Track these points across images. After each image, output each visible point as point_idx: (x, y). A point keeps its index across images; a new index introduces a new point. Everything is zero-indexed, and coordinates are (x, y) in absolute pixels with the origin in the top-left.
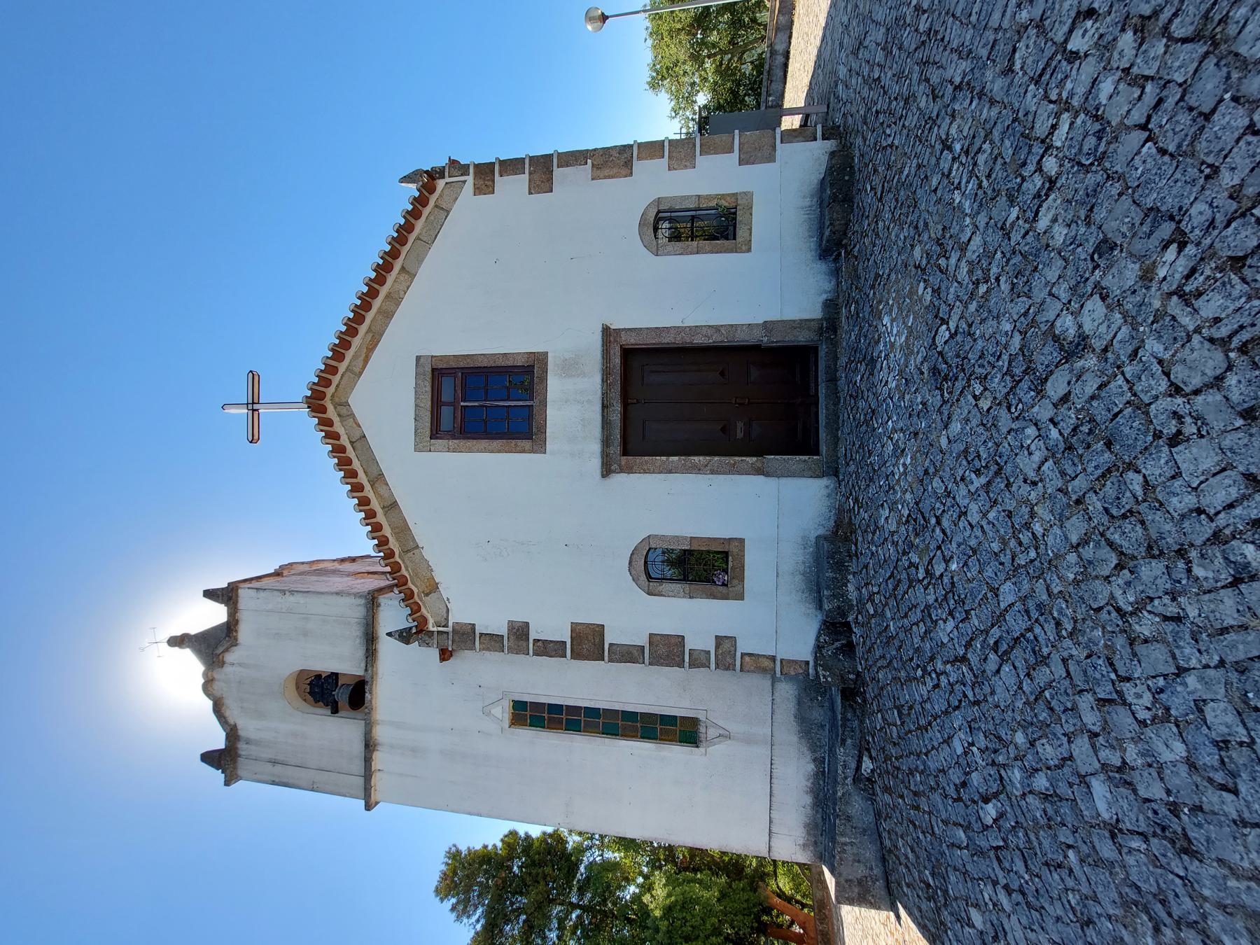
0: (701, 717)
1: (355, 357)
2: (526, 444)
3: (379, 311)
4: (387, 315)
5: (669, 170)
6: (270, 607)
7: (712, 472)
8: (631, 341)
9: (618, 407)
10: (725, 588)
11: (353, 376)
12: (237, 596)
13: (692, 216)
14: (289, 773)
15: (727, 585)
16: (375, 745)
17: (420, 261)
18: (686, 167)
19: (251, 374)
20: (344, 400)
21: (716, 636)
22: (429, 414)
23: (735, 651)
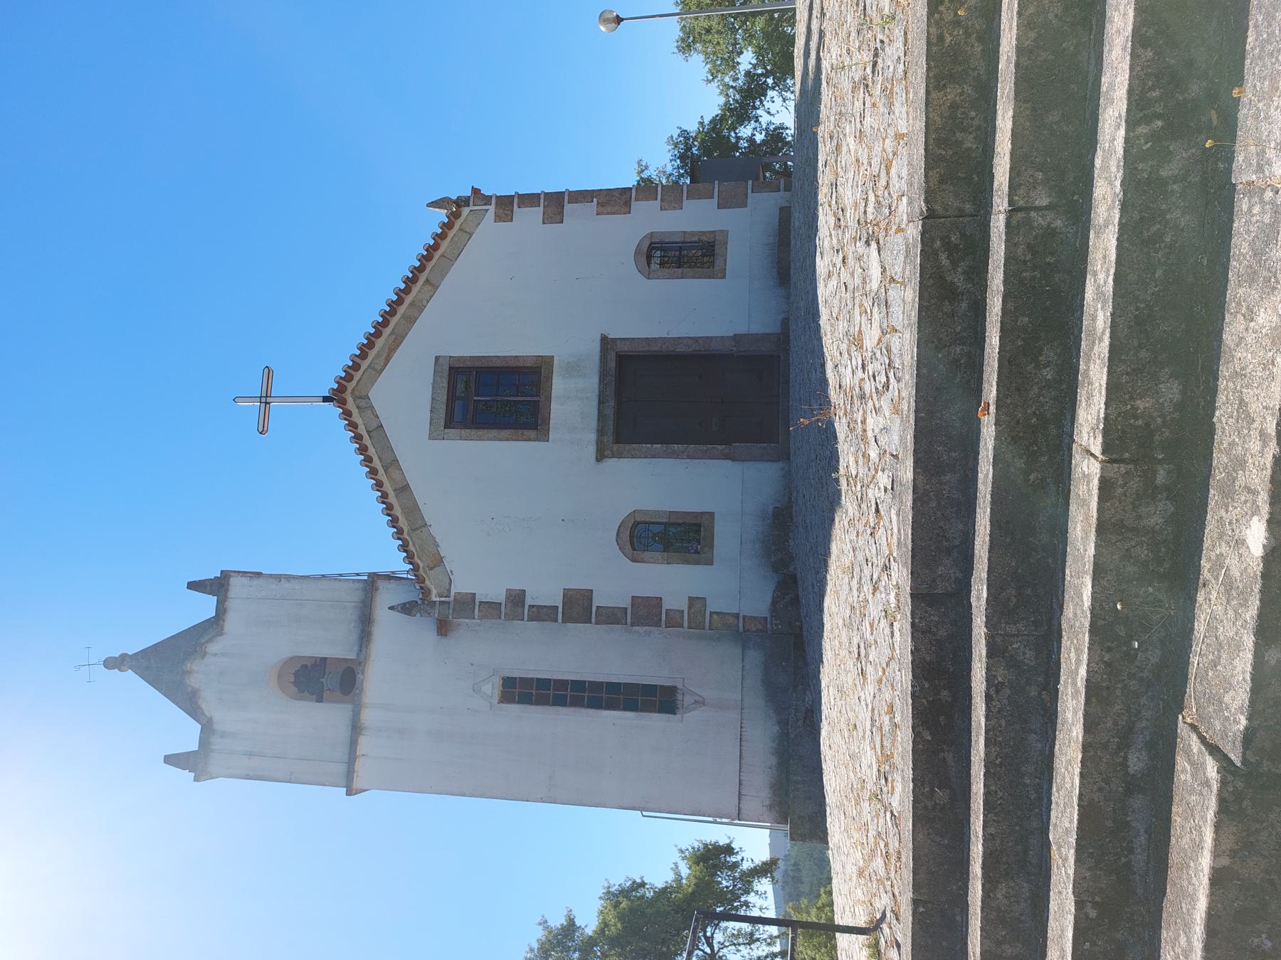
0: (679, 686)
1: (378, 355)
2: (532, 433)
3: (403, 317)
4: (410, 320)
5: (661, 210)
7: (688, 458)
8: (625, 348)
9: (612, 403)
10: (698, 555)
11: (374, 372)
12: (228, 584)
13: (681, 247)
15: (699, 553)
16: (362, 729)
17: (443, 276)
18: (675, 208)
19: (267, 370)
20: (364, 394)
21: (689, 597)
22: (444, 406)
23: (705, 610)
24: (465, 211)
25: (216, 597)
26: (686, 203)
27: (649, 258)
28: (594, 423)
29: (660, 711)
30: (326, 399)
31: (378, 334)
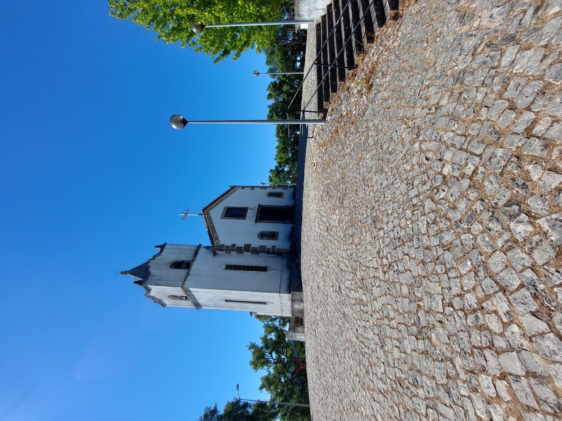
2: (242, 218)
8: (262, 206)
14: (176, 247)
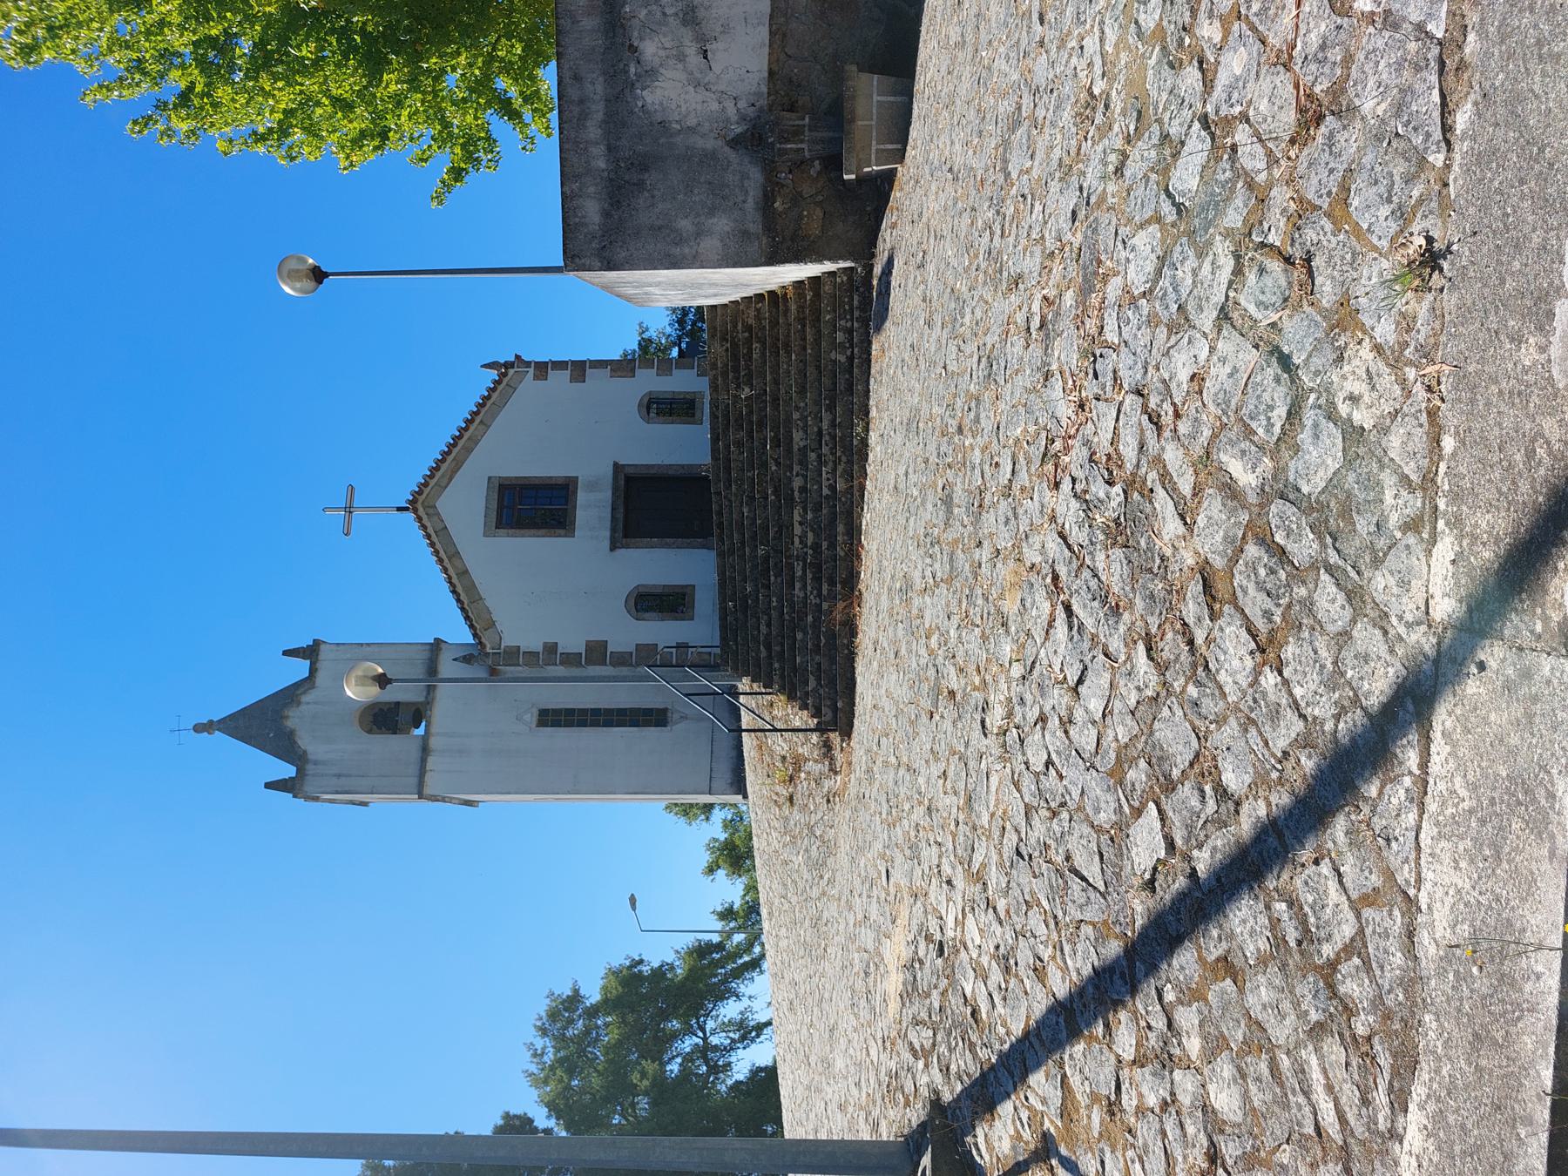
1: (443, 476)
2: (562, 532)
4: (468, 451)
6: (349, 656)
8: (631, 471)
24: (511, 372)
25: (308, 662)
26: (675, 371)
27: (648, 408)
28: (608, 524)
29: (657, 725)
30: (399, 509)
31: (443, 461)
